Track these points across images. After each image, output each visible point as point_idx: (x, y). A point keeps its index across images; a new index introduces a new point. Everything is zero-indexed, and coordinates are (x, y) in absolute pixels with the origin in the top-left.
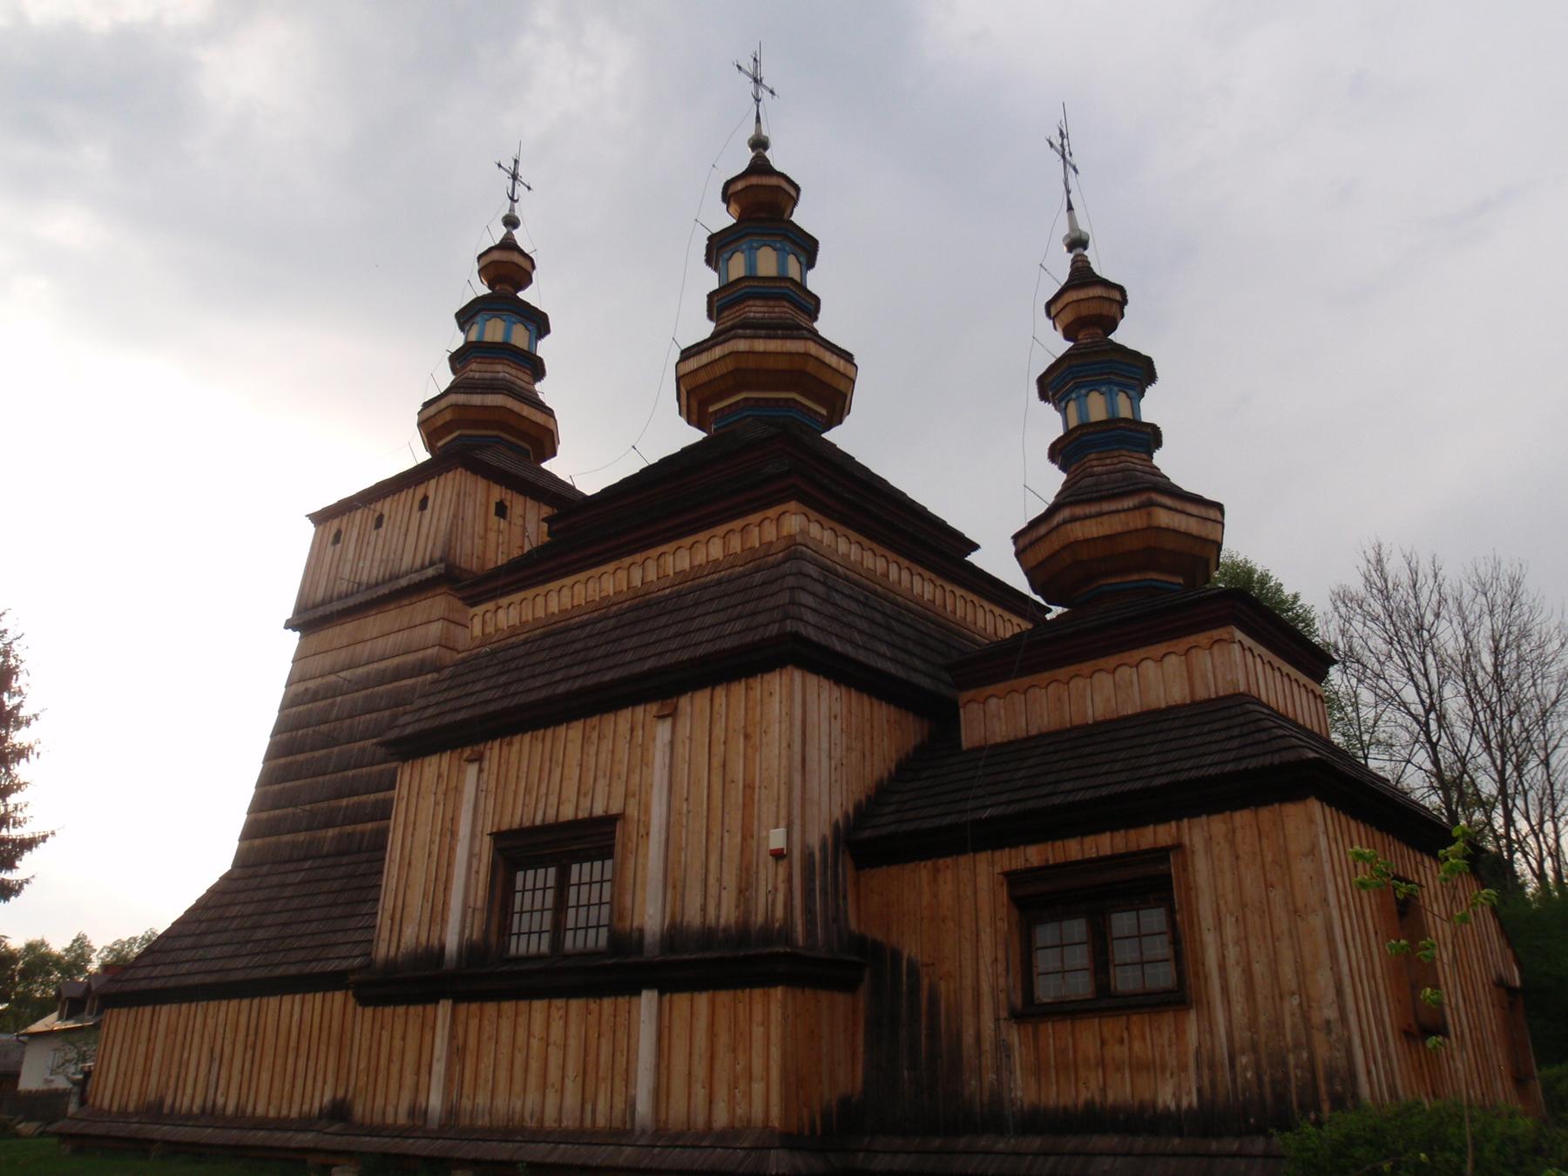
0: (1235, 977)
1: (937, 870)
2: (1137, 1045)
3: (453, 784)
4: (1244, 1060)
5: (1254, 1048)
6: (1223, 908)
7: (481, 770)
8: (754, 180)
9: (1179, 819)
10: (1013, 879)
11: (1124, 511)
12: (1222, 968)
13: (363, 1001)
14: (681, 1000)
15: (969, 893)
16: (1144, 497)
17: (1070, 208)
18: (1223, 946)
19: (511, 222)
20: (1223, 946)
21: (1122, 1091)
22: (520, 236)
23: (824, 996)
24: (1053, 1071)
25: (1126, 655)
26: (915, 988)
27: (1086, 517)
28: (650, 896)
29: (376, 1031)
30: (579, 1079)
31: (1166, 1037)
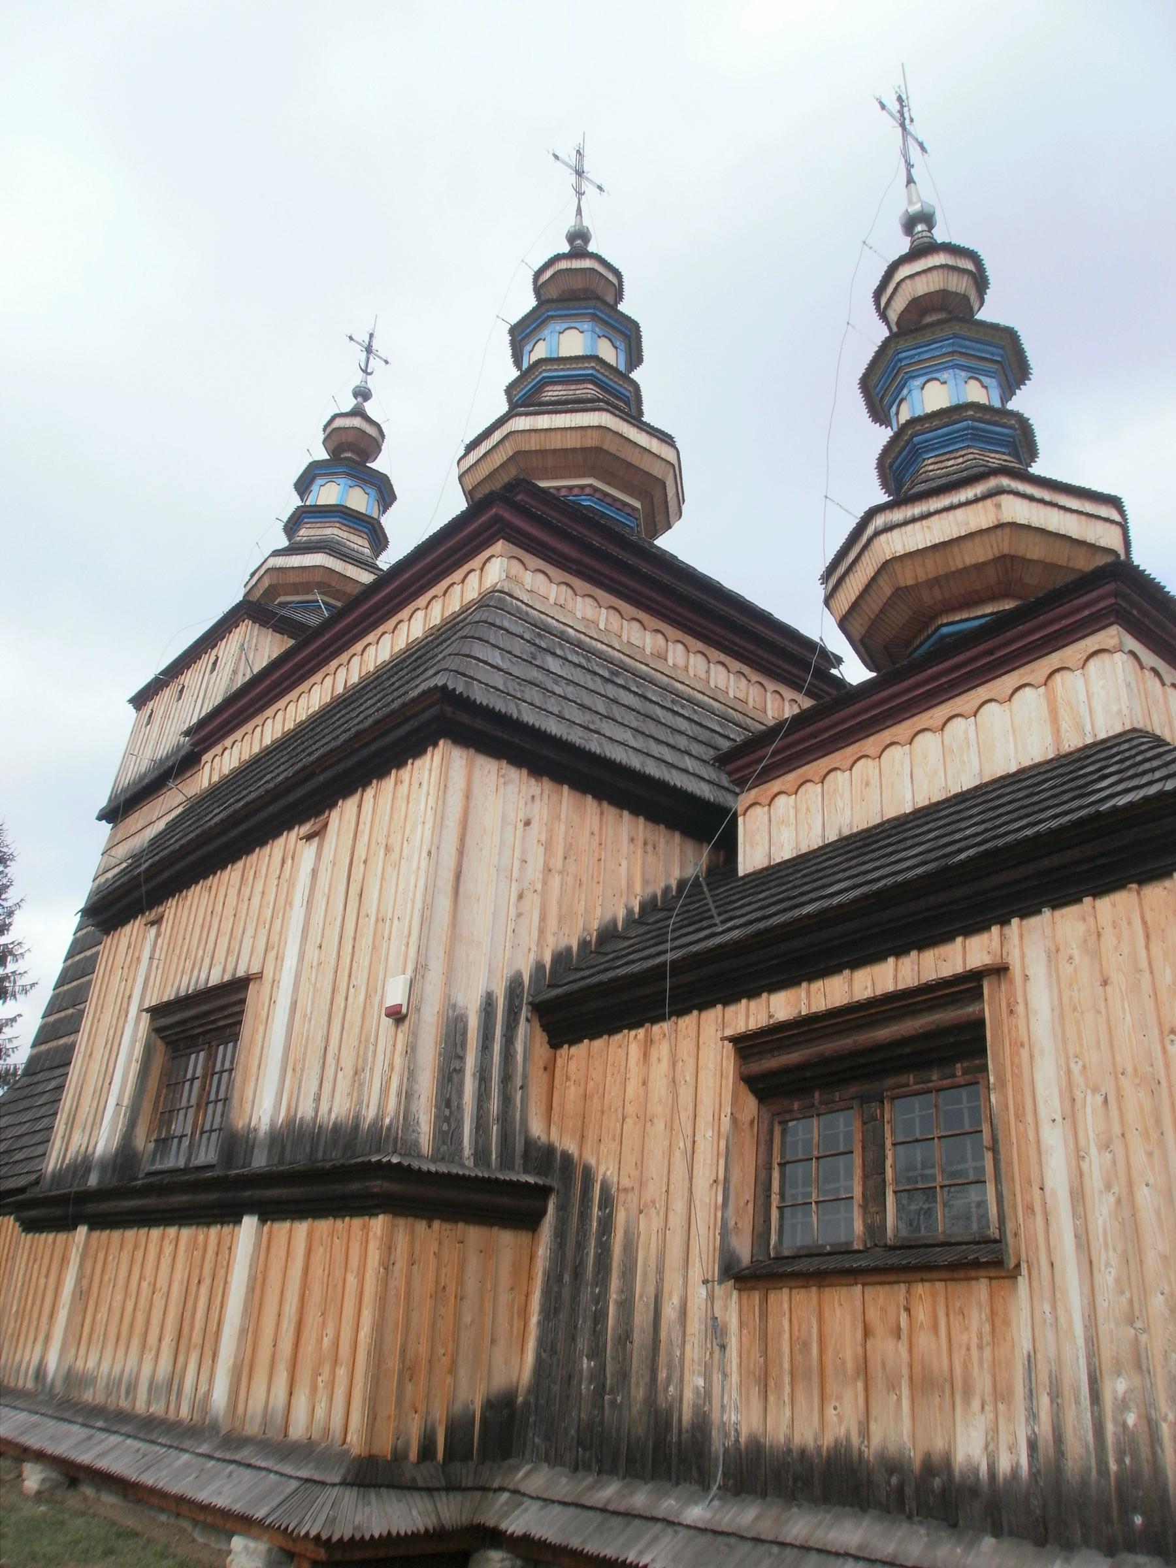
0: (1102, 1211)
1: (649, 1042)
2: (924, 1341)
3: (136, 955)
4: (1121, 1385)
5: (1139, 1363)
6: (1078, 1079)
7: (158, 935)
8: (563, 265)
9: (1004, 922)
10: (746, 1046)
11: (961, 505)
12: (1078, 1195)
13: (31, 1226)
14: (282, 1228)
15: (689, 1077)
16: (992, 483)
17: (910, 181)
18: (1079, 1155)
19: (363, 394)
20: (1079, 1155)
21: (895, 1430)
22: (370, 408)
23: (474, 1234)
24: (787, 1379)
25: (958, 701)
26: (607, 1225)
27: (906, 523)
28: (274, 1088)
29: (30, 1264)
30: (174, 1342)
31: (974, 1328)
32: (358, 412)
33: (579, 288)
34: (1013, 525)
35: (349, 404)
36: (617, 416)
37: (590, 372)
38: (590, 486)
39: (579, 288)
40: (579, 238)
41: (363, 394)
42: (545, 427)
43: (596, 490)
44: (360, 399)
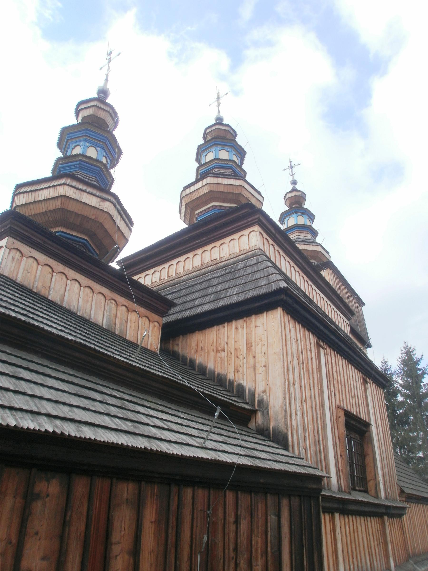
16: (63, 181)
19: (294, 183)
22: (298, 187)
32: (294, 190)
33: (220, 136)
34: (65, 196)
35: (290, 188)
36: (214, 177)
38: (214, 205)
39: (220, 136)
41: (294, 183)
42: (43, 198)
43: (216, 206)
44: (293, 185)
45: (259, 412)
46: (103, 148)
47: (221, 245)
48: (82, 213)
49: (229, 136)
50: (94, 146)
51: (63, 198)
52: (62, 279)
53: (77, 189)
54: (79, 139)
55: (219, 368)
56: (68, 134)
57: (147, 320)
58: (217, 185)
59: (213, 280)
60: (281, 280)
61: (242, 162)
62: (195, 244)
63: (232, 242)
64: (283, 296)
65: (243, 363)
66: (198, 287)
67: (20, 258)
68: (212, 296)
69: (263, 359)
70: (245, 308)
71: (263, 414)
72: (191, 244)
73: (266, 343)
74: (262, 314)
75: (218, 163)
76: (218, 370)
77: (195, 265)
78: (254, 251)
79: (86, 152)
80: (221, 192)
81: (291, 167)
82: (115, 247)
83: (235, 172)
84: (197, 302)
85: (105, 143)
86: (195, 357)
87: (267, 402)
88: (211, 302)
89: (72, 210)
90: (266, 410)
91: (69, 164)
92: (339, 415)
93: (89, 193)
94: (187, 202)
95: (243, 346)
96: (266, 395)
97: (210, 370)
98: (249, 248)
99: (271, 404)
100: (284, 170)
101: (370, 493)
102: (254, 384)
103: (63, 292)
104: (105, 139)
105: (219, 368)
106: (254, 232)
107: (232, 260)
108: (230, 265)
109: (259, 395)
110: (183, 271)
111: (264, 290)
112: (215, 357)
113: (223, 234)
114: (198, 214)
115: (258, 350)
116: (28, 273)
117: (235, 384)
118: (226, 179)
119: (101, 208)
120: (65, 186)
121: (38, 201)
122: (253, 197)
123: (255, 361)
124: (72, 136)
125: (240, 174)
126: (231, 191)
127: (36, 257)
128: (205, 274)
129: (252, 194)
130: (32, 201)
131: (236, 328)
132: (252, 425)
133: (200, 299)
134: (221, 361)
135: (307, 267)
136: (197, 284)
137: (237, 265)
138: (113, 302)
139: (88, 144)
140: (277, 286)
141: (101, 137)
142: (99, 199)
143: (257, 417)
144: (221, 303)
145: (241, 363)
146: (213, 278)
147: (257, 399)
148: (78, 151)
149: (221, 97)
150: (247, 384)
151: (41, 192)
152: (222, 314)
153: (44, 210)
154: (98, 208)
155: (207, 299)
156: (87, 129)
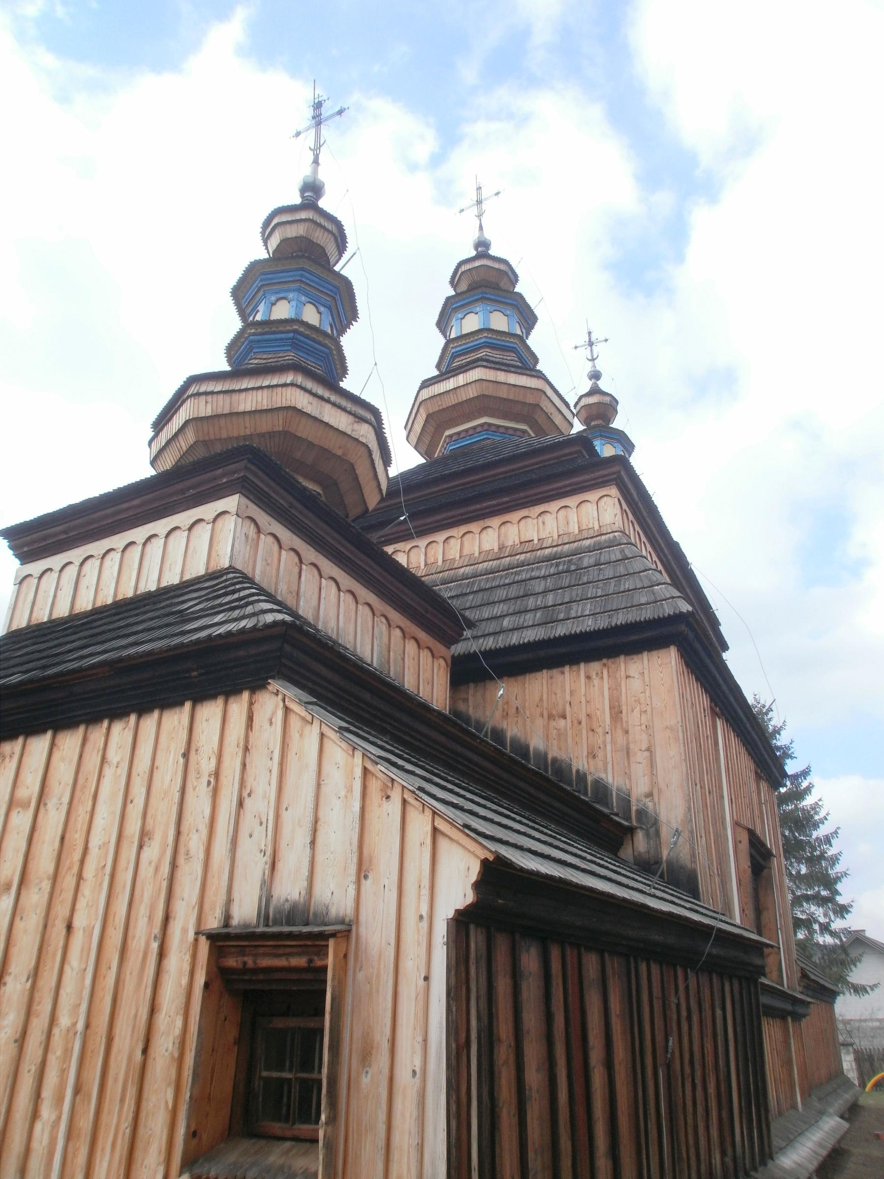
16: (289, 378)
19: (595, 376)
22: (603, 385)
32: (595, 391)
34: (294, 409)
36: (490, 368)
37: (483, 340)
40: (482, 246)
41: (595, 376)
42: (248, 409)
43: (490, 425)
44: (593, 380)
45: (639, 830)
46: (329, 308)
47: (540, 515)
48: (322, 444)
49: (504, 284)
50: (315, 302)
51: (290, 413)
52: (313, 576)
53: (315, 395)
54: (286, 286)
55: (555, 748)
56: (263, 274)
57: (430, 654)
58: (495, 384)
59: (533, 582)
60: (679, 597)
61: (528, 334)
62: (487, 508)
63: (563, 511)
64: (683, 628)
65: (604, 742)
66: (502, 593)
67: (255, 536)
68: (539, 614)
69: (644, 736)
70: (610, 642)
71: (648, 835)
72: (478, 506)
73: (649, 709)
74: (640, 656)
75: (490, 338)
76: (554, 752)
77: (486, 547)
78: (611, 535)
79: (301, 315)
80: (501, 399)
81: (591, 344)
82: (402, 518)
83: (521, 358)
84: (506, 623)
85: (334, 298)
86: (505, 726)
87: (656, 813)
88: (539, 625)
89: (304, 437)
90: (653, 829)
91: (272, 336)
92: (738, 839)
93: (334, 404)
94: (431, 411)
95: (604, 710)
96: (652, 800)
97: (537, 753)
98: (600, 527)
99: (663, 817)
100: (576, 347)
101: (769, 975)
102: (627, 782)
103: (316, 603)
104: (334, 290)
105: (555, 748)
106: (609, 498)
107: (567, 546)
108: (565, 557)
109: (638, 801)
110: (460, 557)
111: (648, 614)
112: (547, 728)
113: (545, 495)
114: (450, 436)
115: (633, 718)
116: (268, 564)
117: (590, 779)
118: (512, 375)
119: (354, 435)
120: (294, 388)
121: (238, 414)
122: (557, 413)
123: (628, 740)
124: (270, 279)
125: (527, 363)
126: (521, 399)
127: (278, 535)
128: (513, 568)
129: (556, 407)
130: (225, 412)
131: (588, 677)
132: (626, 853)
133: (513, 618)
134: (559, 735)
135: (673, 563)
136: (499, 586)
137: (580, 558)
138: (384, 620)
139: (303, 298)
140: (675, 608)
141: (327, 285)
142: (351, 419)
143: (635, 839)
144: (561, 630)
145: (600, 741)
146: (531, 579)
147: (634, 808)
148: (282, 311)
149: (486, 199)
150: (613, 779)
151: (243, 394)
152: (563, 650)
153: (248, 432)
154: (349, 436)
155: (529, 619)
156: (302, 269)
